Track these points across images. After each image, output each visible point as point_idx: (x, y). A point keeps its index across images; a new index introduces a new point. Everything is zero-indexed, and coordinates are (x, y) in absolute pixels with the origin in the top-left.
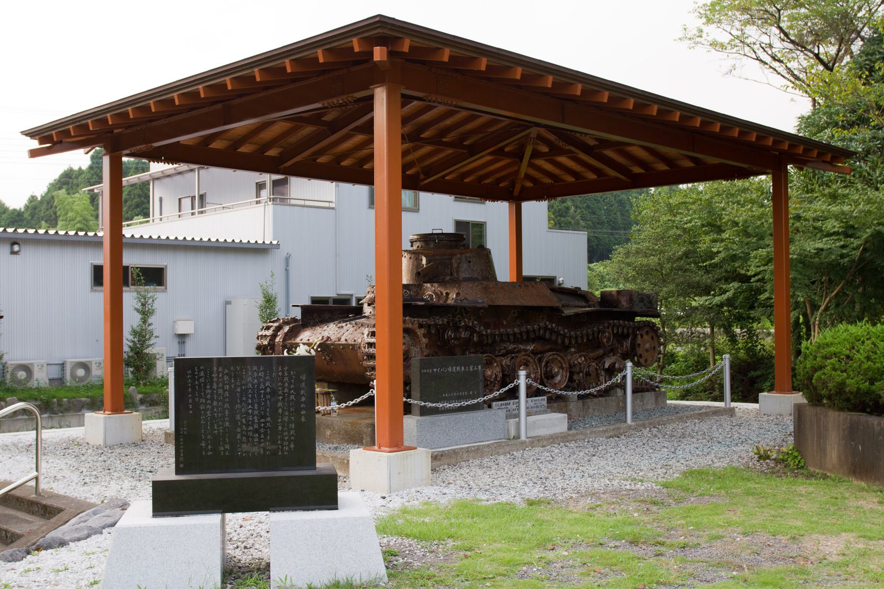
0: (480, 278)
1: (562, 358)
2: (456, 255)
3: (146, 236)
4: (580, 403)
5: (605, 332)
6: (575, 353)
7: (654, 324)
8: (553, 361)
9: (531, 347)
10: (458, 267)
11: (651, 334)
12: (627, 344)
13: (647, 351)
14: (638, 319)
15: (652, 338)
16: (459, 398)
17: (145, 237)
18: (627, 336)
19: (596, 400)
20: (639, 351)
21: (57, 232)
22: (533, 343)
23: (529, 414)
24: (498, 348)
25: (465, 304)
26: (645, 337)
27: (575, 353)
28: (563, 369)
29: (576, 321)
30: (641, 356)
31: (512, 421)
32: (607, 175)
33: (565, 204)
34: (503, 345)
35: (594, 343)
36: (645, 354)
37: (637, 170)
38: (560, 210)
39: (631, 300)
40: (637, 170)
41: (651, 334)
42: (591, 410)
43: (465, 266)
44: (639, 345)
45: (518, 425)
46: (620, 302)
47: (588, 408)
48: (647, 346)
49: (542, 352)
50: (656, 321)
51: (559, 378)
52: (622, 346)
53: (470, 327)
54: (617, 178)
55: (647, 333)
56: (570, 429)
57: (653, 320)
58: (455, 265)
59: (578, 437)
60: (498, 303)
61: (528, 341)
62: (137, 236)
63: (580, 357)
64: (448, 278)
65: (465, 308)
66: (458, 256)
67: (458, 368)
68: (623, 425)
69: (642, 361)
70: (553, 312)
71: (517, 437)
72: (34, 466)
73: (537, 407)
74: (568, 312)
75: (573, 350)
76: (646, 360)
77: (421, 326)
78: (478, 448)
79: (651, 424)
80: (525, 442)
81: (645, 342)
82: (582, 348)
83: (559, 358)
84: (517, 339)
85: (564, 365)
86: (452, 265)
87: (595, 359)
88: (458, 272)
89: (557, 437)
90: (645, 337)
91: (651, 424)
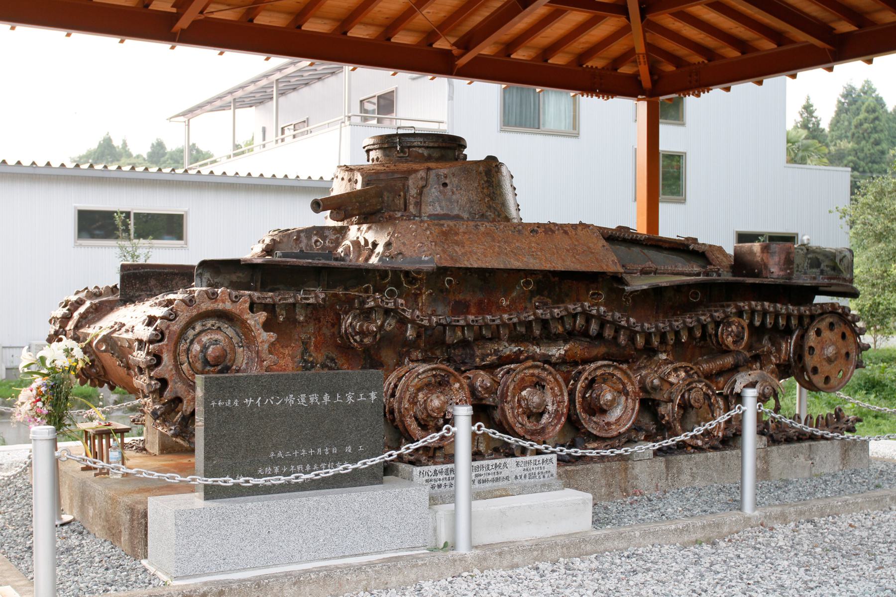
0: (465, 216)
1: (624, 372)
2: (416, 171)
3: (243, 174)
4: (660, 463)
5: (730, 324)
6: (666, 362)
7: (846, 311)
8: (605, 379)
9: (557, 351)
10: (421, 194)
11: (838, 330)
12: (788, 346)
13: (829, 360)
14: (819, 299)
15: (843, 336)
16: (316, 461)
17: (241, 174)
18: (788, 332)
19: (699, 457)
20: (810, 361)
21: (119, 168)
22: (566, 341)
23: (477, 496)
24: (478, 352)
25: (400, 264)
26: (826, 334)
27: (666, 362)
28: (627, 394)
29: (657, 299)
30: (815, 370)
31: (443, 510)
32: (792, 42)
33: (879, 148)
34: (491, 347)
35: (705, 344)
36: (825, 369)
37: (845, 27)
38: (872, 154)
39: (789, 261)
40: (845, 27)
41: (840, 328)
42: (686, 477)
43: (433, 191)
44: (812, 349)
45: (454, 515)
46: (766, 266)
47: (680, 472)
48: (830, 351)
49: (586, 361)
50: (852, 305)
51: (617, 412)
52: (779, 350)
53: (392, 310)
54: (812, 46)
55: (831, 326)
56: (597, 522)
57: (843, 302)
58: (413, 192)
59: (609, 545)
60: (466, 264)
61: (551, 338)
62: (231, 173)
63: (676, 370)
64: (399, 214)
65: (407, 273)
66: (422, 174)
67: (314, 398)
68: (735, 516)
69: (818, 380)
70: (611, 284)
71: (449, 546)
72: (62, 467)
73: (532, 476)
74: (639, 284)
75: (663, 356)
76: (827, 379)
77: (253, 307)
78: (329, 572)
79: (801, 513)
80: (463, 559)
81: (824, 344)
82: (682, 351)
83: (619, 374)
84: (522, 334)
85: (630, 388)
86: (405, 188)
87: (709, 377)
88: (418, 204)
89: (552, 546)
90: (826, 334)
91: (801, 513)
